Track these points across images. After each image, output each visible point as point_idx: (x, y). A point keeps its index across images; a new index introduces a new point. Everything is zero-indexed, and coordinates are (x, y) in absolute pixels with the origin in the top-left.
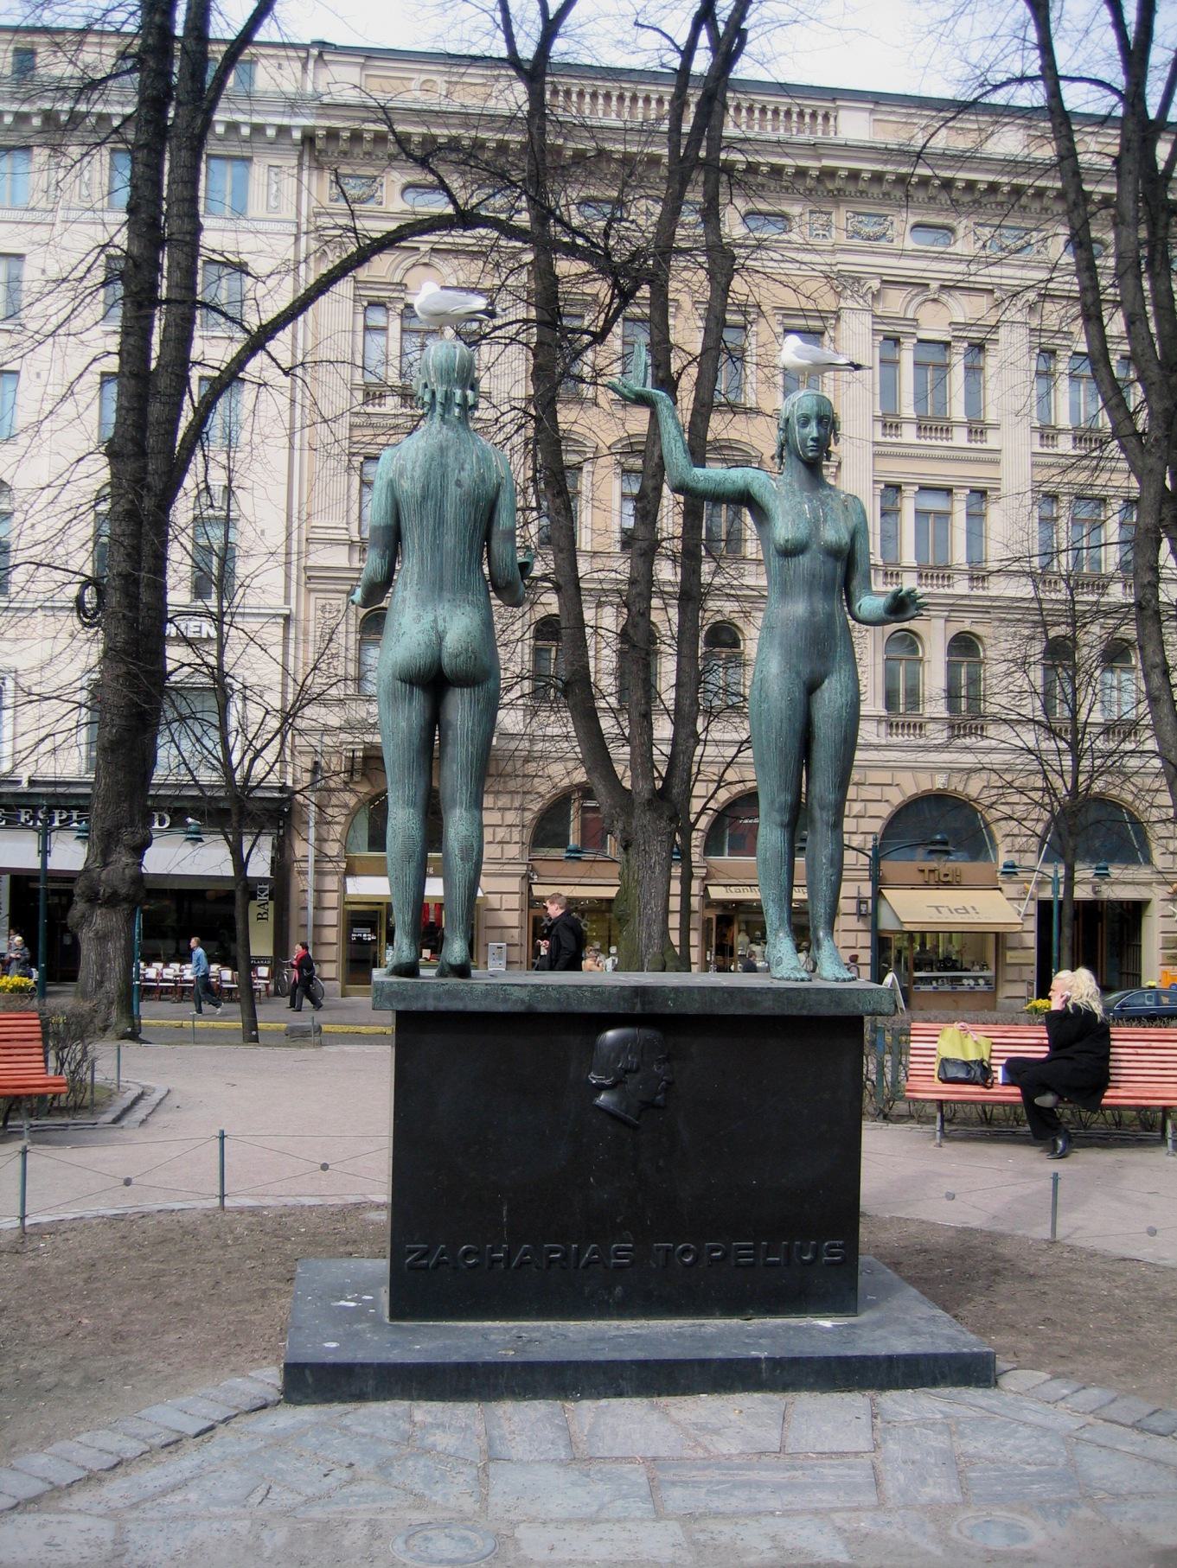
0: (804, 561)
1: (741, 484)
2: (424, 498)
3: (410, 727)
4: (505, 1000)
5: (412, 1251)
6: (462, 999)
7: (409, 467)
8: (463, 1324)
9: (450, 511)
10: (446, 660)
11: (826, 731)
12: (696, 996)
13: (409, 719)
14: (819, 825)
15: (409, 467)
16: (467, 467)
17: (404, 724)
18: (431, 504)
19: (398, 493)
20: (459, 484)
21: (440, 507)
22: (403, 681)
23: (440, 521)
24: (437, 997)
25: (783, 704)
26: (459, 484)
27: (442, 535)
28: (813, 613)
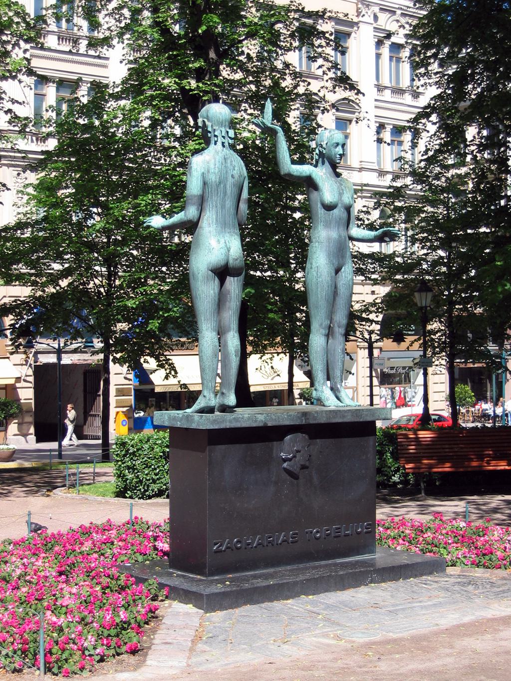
0: (336, 211)
1: (308, 173)
2: (220, 183)
3: (215, 293)
4: (256, 421)
5: (216, 544)
6: (240, 422)
7: (212, 166)
8: (243, 574)
9: (229, 192)
10: (231, 262)
11: (342, 290)
12: (324, 415)
13: (214, 289)
14: (337, 335)
15: (212, 166)
16: (236, 168)
17: (212, 292)
18: (222, 185)
19: (207, 179)
20: (232, 176)
21: (225, 187)
22: (212, 271)
23: (225, 193)
24: (230, 421)
25: (329, 279)
26: (232, 176)
27: (225, 202)
28: (340, 236)
